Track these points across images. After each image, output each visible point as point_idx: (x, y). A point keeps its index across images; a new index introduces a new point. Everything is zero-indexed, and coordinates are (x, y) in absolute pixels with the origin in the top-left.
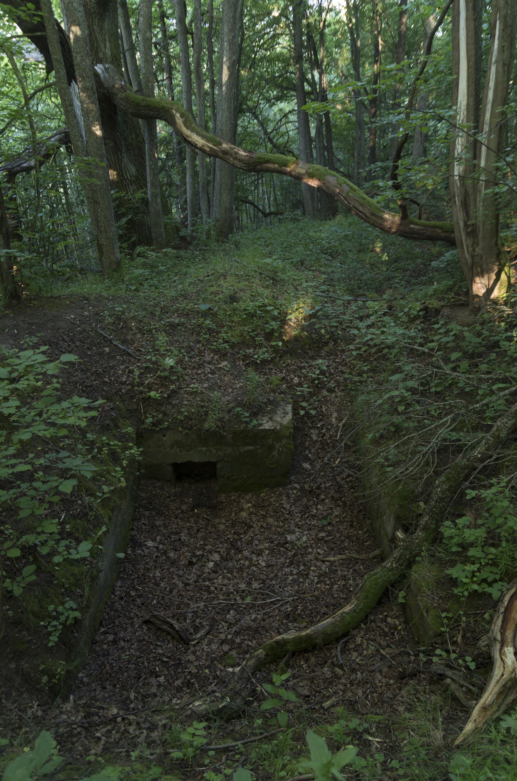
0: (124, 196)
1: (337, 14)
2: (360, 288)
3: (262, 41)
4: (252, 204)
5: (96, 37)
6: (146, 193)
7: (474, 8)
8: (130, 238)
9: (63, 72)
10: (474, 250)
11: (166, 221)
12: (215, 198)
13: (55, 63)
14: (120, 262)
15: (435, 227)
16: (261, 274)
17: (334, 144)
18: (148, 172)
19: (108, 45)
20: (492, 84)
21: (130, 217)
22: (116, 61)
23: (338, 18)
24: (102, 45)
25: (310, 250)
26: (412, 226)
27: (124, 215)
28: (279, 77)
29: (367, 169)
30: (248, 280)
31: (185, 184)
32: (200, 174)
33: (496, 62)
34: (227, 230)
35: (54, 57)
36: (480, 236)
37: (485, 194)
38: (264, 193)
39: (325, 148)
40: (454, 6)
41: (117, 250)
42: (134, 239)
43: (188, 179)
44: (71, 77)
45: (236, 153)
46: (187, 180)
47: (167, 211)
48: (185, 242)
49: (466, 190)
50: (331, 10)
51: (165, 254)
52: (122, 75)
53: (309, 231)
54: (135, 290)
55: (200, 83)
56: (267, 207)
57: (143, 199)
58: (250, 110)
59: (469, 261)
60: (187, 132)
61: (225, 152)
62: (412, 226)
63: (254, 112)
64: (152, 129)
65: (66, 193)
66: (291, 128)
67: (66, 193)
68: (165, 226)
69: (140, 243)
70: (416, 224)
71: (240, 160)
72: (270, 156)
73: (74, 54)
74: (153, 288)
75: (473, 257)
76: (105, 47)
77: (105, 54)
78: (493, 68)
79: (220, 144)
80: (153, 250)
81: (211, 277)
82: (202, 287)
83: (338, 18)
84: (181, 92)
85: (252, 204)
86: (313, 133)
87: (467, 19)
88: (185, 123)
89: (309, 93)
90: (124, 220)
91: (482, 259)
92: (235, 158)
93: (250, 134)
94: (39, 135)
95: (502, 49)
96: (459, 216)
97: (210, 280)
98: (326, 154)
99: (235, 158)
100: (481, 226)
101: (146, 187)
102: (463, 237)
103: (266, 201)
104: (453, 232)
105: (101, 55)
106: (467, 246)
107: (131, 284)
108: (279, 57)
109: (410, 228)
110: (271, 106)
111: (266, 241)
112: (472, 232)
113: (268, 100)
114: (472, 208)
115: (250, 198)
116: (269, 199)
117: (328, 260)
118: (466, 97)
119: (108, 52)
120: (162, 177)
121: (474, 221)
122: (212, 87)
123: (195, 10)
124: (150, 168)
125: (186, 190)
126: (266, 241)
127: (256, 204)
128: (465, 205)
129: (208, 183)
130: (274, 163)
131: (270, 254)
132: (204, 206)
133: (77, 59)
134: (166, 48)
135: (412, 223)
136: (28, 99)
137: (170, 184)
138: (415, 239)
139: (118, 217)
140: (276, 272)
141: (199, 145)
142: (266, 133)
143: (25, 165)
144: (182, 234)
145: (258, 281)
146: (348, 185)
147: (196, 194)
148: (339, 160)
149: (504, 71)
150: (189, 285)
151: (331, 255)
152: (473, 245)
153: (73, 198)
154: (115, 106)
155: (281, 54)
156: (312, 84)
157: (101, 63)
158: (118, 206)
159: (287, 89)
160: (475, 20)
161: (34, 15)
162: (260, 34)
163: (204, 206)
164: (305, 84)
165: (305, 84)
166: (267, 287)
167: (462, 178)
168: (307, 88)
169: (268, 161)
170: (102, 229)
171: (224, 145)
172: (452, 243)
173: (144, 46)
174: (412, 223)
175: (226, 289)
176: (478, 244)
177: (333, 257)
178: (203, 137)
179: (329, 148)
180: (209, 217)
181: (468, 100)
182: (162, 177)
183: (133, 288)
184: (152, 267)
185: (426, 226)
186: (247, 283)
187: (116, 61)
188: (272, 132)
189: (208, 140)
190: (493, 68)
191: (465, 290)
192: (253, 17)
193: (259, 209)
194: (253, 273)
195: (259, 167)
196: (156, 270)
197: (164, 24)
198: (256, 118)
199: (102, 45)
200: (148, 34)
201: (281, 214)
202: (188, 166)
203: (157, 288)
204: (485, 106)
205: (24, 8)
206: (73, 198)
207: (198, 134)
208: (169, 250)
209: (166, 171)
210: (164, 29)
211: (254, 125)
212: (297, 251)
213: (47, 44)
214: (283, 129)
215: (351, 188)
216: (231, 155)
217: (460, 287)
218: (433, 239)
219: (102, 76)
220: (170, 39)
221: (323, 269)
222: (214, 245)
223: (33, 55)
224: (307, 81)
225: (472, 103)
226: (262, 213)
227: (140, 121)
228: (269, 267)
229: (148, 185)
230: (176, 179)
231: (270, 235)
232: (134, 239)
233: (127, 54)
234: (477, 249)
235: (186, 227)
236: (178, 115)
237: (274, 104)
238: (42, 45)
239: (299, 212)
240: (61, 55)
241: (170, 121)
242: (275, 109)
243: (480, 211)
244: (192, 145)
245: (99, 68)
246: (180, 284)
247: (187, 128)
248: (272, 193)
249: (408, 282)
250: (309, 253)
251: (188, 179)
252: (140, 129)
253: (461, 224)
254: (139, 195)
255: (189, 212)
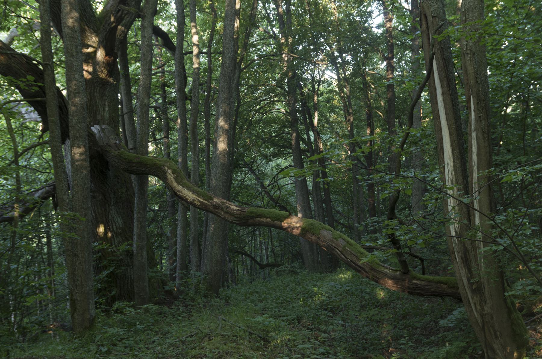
0: (108, 248)
1: (329, 85)
2: (365, 349)
3: (258, 107)
4: (250, 256)
5: (96, 102)
6: (131, 245)
7: (449, 85)
8: (110, 292)
9: (58, 132)
10: (483, 309)
11: (151, 274)
12: (206, 250)
13: (50, 124)
14: (94, 319)
15: (440, 282)
16: (251, 334)
17: (333, 197)
18: (135, 224)
19: (107, 109)
20: (474, 149)
21: (111, 269)
22: (114, 123)
23: (330, 88)
24: (101, 109)
25: (309, 306)
26: (415, 281)
27: (105, 268)
28: (276, 136)
29: (364, 224)
30: (235, 341)
31: (176, 236)
32: (192, 226)
33: (475, 130)
34: (218, 284)
35: (50, 119)
36: (487, 293)
37: (485, 252)
38: (260, 245)
39: (324, 201)
40: (430, 84)
41: (92, 306)
42: (113, 293)
43: (179, 231)
44: (65, 136)
45: (228, 208)
46: (178, 232)
47: (152, 262)
48: (169, 298)
49: (464, 246)
50: (324, 82)
51: (147, 311)
52: (118, 134)
53: (307, 285)
54: (106, 352)
55: (196, 141)
56: (265, 258)
57: (128, 251)
58: (246, 165)
59: (480, 320)
60: (177, 187)
61: (216, 207)
62: (415, 281)
63: (251, 167)
64: (144, 183)
65: (49, 243)
66: (288, 183)
67: (49, 243)
68: (150, 279)
69: (120, 298)
70: (419, 279)
71: (231, 214)
72: (262, 210)
73: (70, 117)
74: (128, 349)
75: (482, 316)
76: (104, 110)
77: (103, 116)
78: (474, 135)
79: (212, 199)
80: (133, 306)
81: (193, 338)
82: (183, 350)
83: (330, 88)
84: (176, 149)
85: (250, 256)
86: (310, 186)
87: (443, 94)
88: (176, 179)
89: (305, 151)
90: (105, 273)
91: (492, 318)
92: (226, 213)
93: (246, 187)
94: (25, 188)
95: (479, 119)
96: (461, 273)
97: (193, 341)
98: (324, 205)
99: (226, 213)
100: (486, 283)
101: (132, 239)
102: (469, 294)
103: (264, 252)
104: (458, 288)
105: (99, 117)
106: (475, 304)
107: (103, 345)
108: (275, 120)
109: (413, 284)
110: (268, 162)
111: (260, 296)
112: (478, 290)
113: (265, 157)
114: (473, 264)
115: (247, 248)
116: (267, 249)
117: (329, 316)
118: (452, 159)
119: (107, 115)
120: (153, 228)
121: (477, 279)
122: (208, 145)
123: (194, 81)
124: (138, 221)
125: (176, 241)
126: (260, 296)
127: (253, 256)
128: (466, 261)
129: (200, 234)
130: (267, 218)
131: (263, 311)
132: (194, 257)
133: (73, 121)
134: (165, 111)
135: (414, 278)
136: (17, 155)
137: (161, 235)
138: (421, 295)
139: (98, 269)
140: (268, 332)
141: (190, 199)
142: (263, 186)
143: (7, 216)
144: (167, 288)
145: (247, 342)
146: (344, 240)
147: (186, 247)
148: (338, 212)
149: (485, 138)
150: (169, 347)
151: (331, 310)
152: (480, 303)
153: (55, 248)
154: (107, 162)
155: (278, 117)
156: (308, 142)
157: (98, 124)
158: (100, 259)
159: (283, 147)
160: (451, 95)
161: (33, 85)
162: (257, 101)
163: (194, 257)
164: (301, 143)
165: (301, 143)
166: (258, 349)
167: (459, 235)
168: (303, 146)
169: (260, 216)
170: (78, 283)
171: (216, 200)
172: (459, 299)
173: (141, 111)
174: (414, 278)
175: (210, 352)
176: (485, 303)
177: (334, 313)
178: (194, 192)
179: (328, 201)
180: (199, 270)
181: (454, 162)
182: (153, 228)
183: (104, 350)
184: (131, 325)
185: (429, 281)
186: (234, 345)
187: (114, 123)
188: (269, 185)
189: (199, 195)
190: (474, 135)
191: (480, 352)
192: (250, 86)
193: (256, 261)
194: (242, 333)
195: (251, 221)
196: (133, 329)
197: (164, 91)
198: (253, 172)
199: (101, 109)
200: (146, 101)
201: (278, 266)
202: (179, 218)
203: (131, 350)
204: (471, 167)
205: (24, 80)
206: (55, 248)
207: (189, 189)
208: (151, 306)
209: (158, 222)
210: (164, 96)
211: (250, 180)
212: (293, 307)
213: (46, 108)
214: (280, 183)
215: (348, 242)
216: (222, 210)
217: (475, 349)
218: (442, 295)
219: (97, 135)
220: (170, 104)
221: (323, 327)
222: (200, 300)
223: (30, 115)
224: (303, 140)
225: (458, 165)
226: (259, 264)
227: (133, 177)
228: (260, 327)
229: (135, 237)
230: (167, 230)
231: (265, 289)
232: (113, 293)
233: (125, 116)
234: (485, 308)
235: (174, 279)
236: (170, 171)
237: (270, 160)
238: (41, 108)
239: (296, 265)
240: (58, 118)
241: (162, 176)
242: (273, 164)
243: (482, 268)
244: (182, 199)
245: (95, 129)
246: (160, 344)
247: (178, 183)
248: (270, 243)
249: (418, 341)
250: (307, 309)
251: (179, 231)
252: (131, 183)
253: (465, 281)
254: (124, 247)
255: (178, 264)
